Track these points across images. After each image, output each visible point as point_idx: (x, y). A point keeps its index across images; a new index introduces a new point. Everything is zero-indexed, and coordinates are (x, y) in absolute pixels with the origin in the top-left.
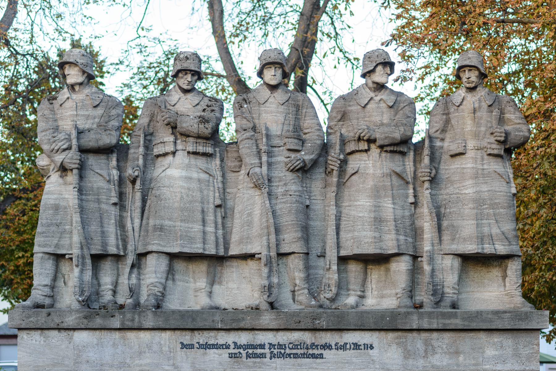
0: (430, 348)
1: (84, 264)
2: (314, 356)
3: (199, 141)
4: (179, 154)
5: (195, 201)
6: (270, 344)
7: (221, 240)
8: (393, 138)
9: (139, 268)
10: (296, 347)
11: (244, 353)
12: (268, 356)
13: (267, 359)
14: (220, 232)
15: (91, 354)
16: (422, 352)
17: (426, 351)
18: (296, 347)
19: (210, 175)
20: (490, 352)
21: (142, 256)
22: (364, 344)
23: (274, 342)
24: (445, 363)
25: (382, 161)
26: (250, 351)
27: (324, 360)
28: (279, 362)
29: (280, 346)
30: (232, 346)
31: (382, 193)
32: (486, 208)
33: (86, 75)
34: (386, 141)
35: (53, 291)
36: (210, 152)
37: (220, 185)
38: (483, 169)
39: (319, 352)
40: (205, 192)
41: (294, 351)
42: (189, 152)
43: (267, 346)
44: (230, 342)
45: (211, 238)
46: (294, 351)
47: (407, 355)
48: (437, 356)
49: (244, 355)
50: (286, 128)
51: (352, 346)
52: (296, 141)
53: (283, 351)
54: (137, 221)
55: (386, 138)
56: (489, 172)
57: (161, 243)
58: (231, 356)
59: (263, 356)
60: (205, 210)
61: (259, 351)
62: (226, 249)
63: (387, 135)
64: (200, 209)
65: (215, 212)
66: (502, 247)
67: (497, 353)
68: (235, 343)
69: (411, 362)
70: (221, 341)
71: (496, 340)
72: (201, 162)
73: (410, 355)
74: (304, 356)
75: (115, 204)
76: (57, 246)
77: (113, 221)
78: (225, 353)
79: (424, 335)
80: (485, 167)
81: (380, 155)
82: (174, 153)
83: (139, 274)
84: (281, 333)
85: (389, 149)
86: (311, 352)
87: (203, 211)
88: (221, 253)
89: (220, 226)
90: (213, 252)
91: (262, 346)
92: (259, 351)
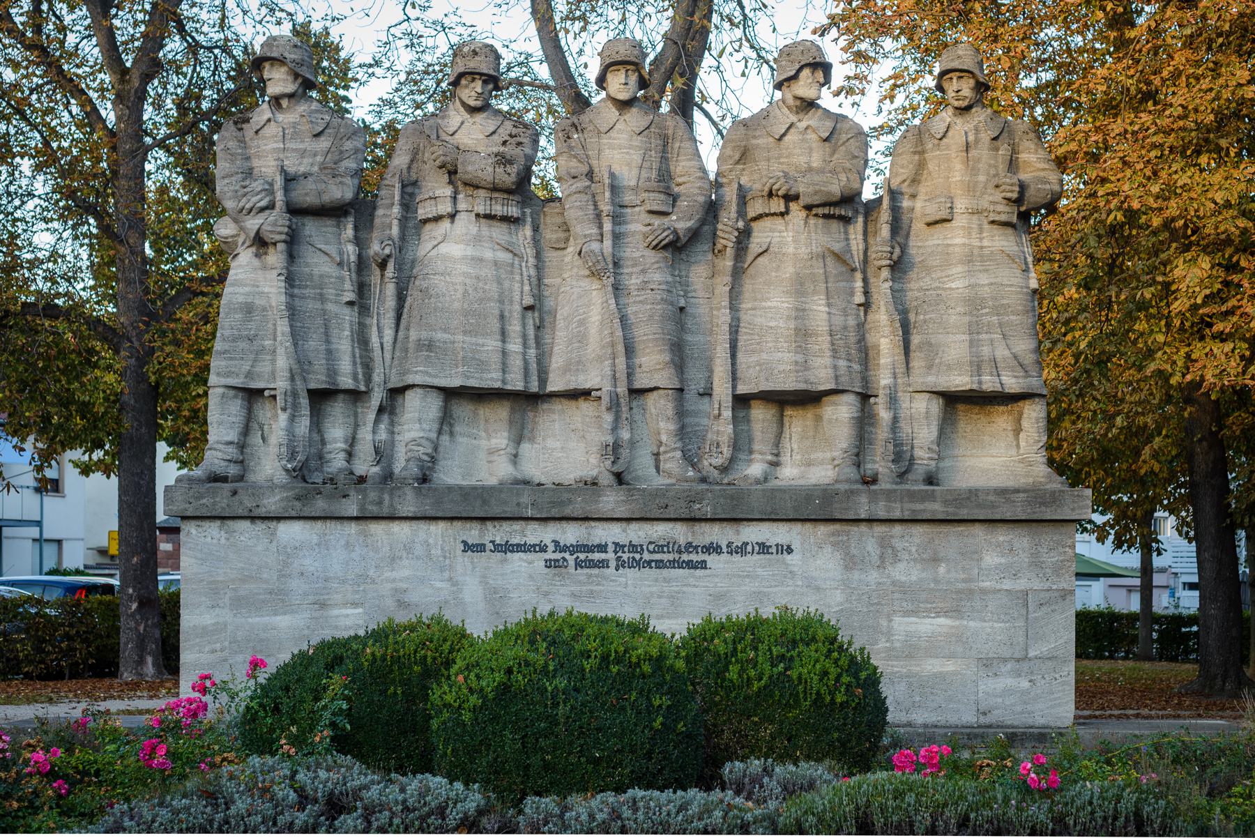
0: (890, 551)
1: (295, 406)
2: (690, 565)
3: (496, 195)
4: (462, 218)
5: (489, 299)
6: (616, 544)
7: (533, 367)
8: (829, 193)
9: (392, 413)
10: (660, 549)
11: (571, 559)
12: (613, 564)
13: (612, 570)
14: (532, 352)
15: (307, 561)
16: (875, 559)
17: (882, 557)
18: (660, 549)
19: (515, 255)
20: (991, 559)
21: (396, 393)
22: (777, 545)
23: (623, 540)
24: (914, 578)
25: (809, 232)
26: (582, 556)
27: (708, 571)
28: (631, 574)
29: (633, 548)
30: (551, 547)
31: (809, 287)
32: (987, 314)
33: (300, 80)
34: (816, 197)
35: (242, 453)
36: (515, 215)
37: (533, 272)
38: (982, 247)
39: (701, 557)
40: (506, 284)
41: (657, 557)
42: (478, 215)
43: (611, 548)
44: (547, 540)
45: (516, 363)
46: (657, 557)
47: (851, 563)
48: (901, 566)
49: (572, 563)
50: (644, 175)
51: (757, 548)
52: (662, 197)
53: (637, 556)
54: (388, 334)
55: (816, 193)
56: (992, 252)
57: (430, 370)
58: (549, 564)
59: (603, 564)
60: (506, 314)
61: (597, 556)
62: (543, 381)
63: (817, 188)
64: (497, 312)
65: (523, 317)
66: (1013, 380)
67: (1003, 561)
68: (556, 543)
69: (856, 575)
70: (532, 540)
71: (1001, 539)
72: (499, 232)
73: (854, 564)
74: (674, 564)
75: (351, 303)
76: (249, 375)
77: (347, 333)
78: (538, 560)
79: (879, 529)
80: (986, 243)
81: (806, 223)
82: (452, 216)
83: (392, 423)
84: (634, 526)
85: (820, 211)
86: (685, 557)
87: (502, 317)
88: (534, 387)
89: (532, 342)
90: (519, 386)
91: (602, 548)
92: (597, 556)
